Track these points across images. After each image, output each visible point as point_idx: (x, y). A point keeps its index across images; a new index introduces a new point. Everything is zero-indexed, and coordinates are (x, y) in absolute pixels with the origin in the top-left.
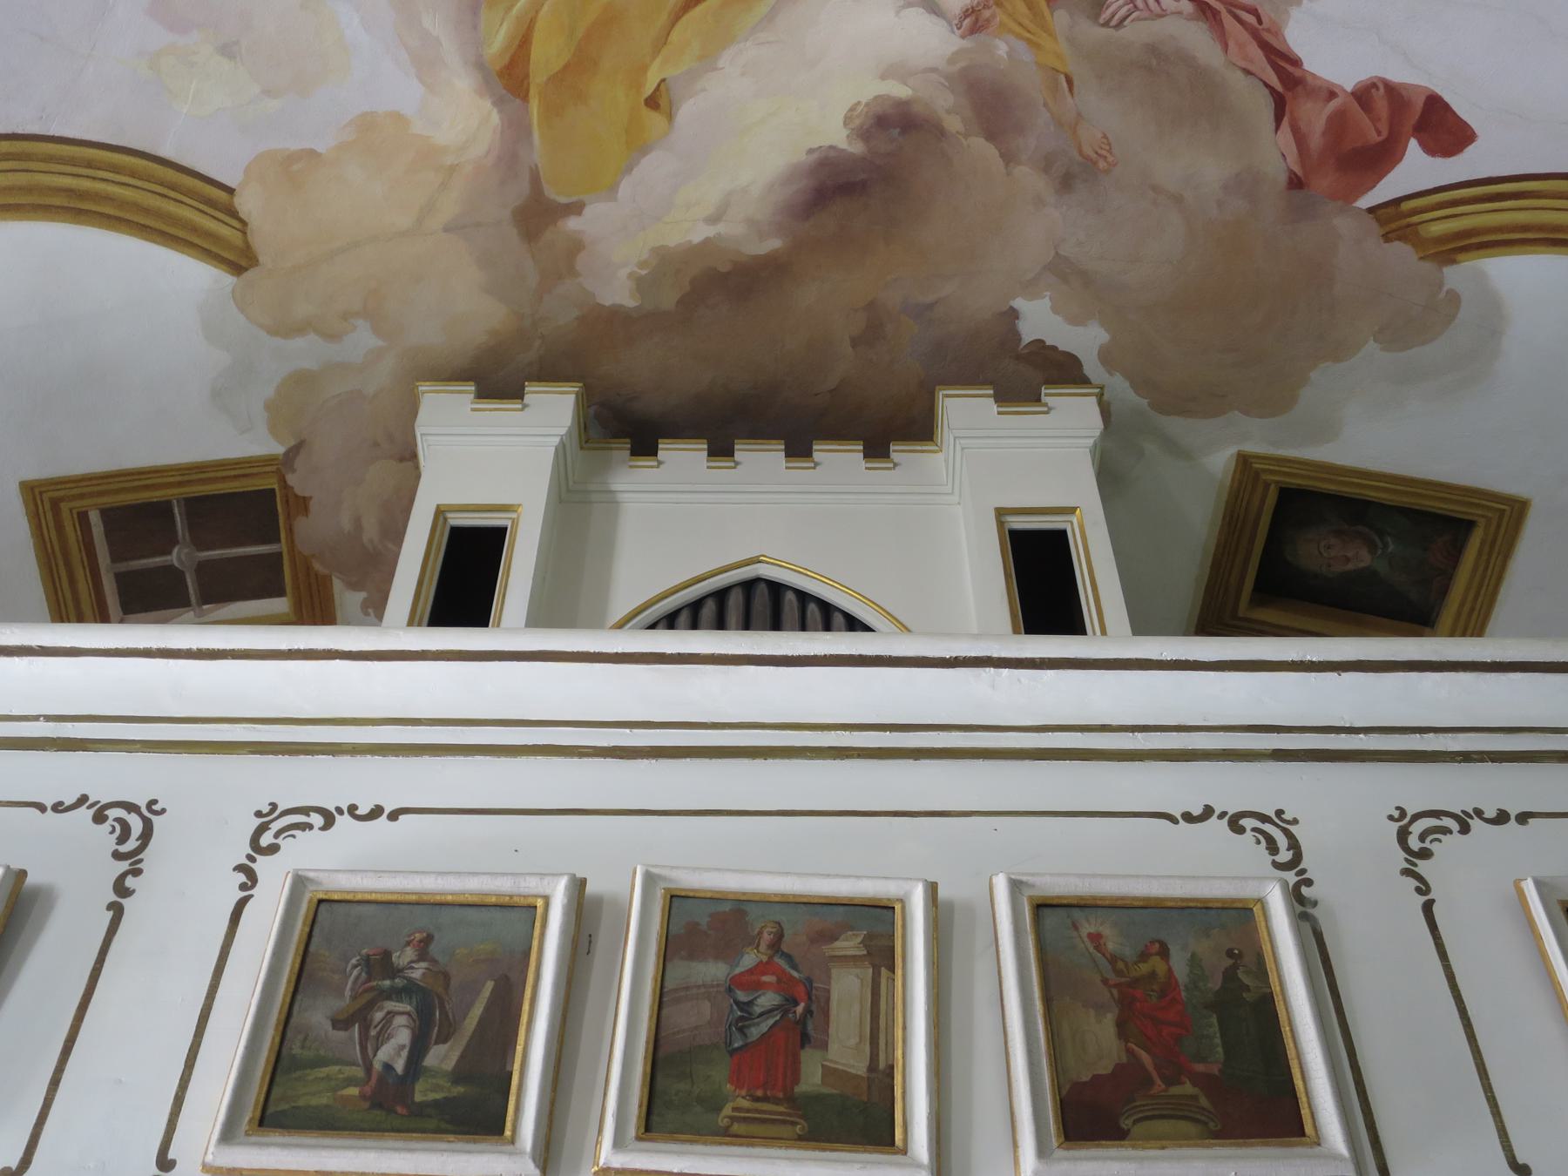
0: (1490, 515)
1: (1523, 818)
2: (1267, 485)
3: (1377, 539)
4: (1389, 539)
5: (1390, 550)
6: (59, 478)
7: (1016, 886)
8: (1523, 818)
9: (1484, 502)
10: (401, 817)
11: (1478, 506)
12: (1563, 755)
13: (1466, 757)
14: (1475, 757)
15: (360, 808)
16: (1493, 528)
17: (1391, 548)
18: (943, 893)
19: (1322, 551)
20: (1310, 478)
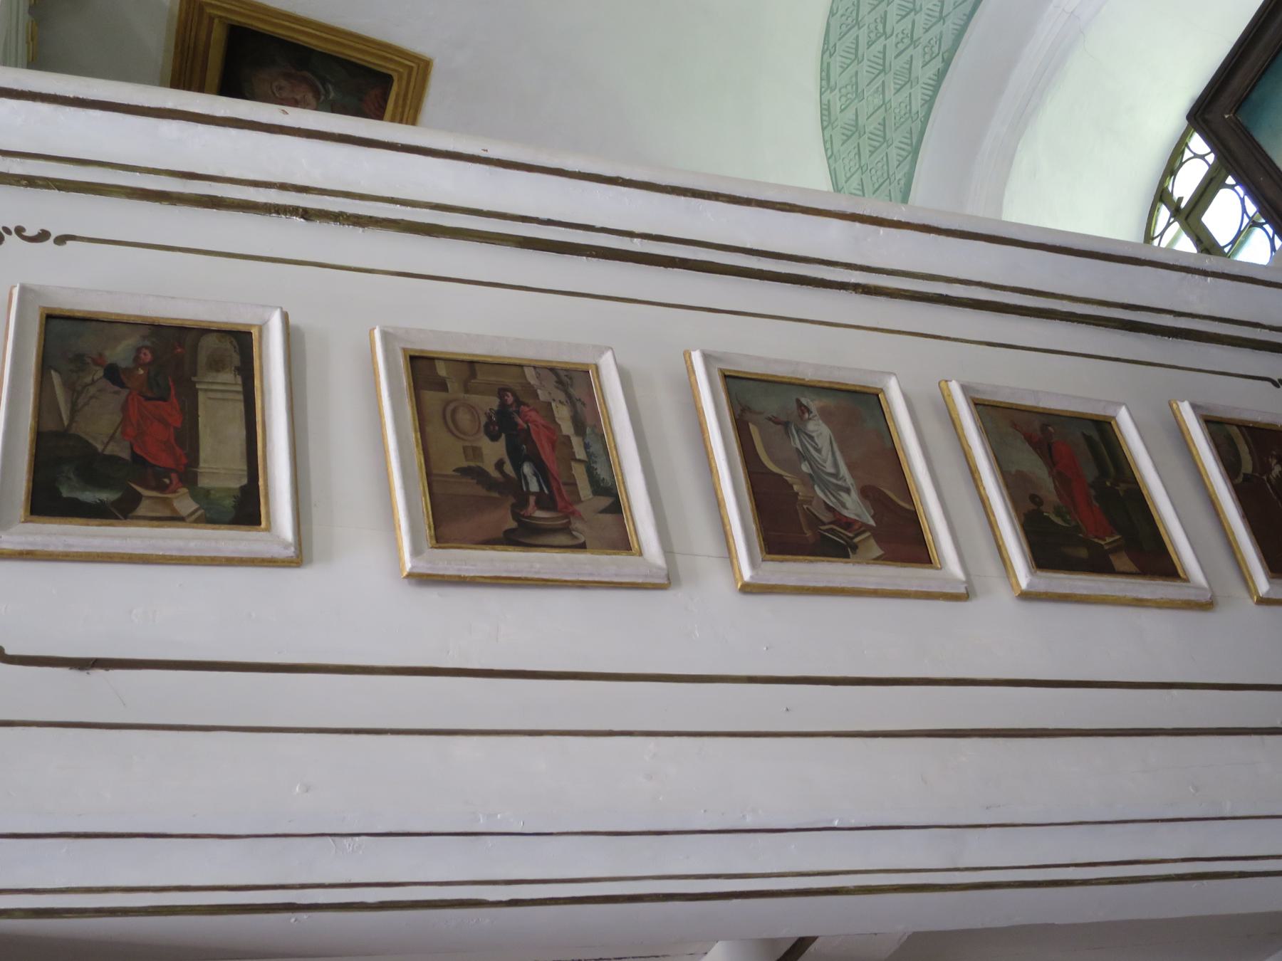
0: (401, 70)
1: (61, 240)
2: (211, 19)
3: (320, 86)
4: (330, 87)
5: (331, 97)
6: (1050, 409)
7: (386, 336)
8: (61, 240)
9: (396, 58)
10: (69, 243)
11: (391, 60)
12: (129, 191)
13: (31, 182)
14: (40, 183)
15: (27, 231)
16: (404, 83)
17: (332, 95)
18: (292, 321)
19: (275, 91)
20: (249, 17)
